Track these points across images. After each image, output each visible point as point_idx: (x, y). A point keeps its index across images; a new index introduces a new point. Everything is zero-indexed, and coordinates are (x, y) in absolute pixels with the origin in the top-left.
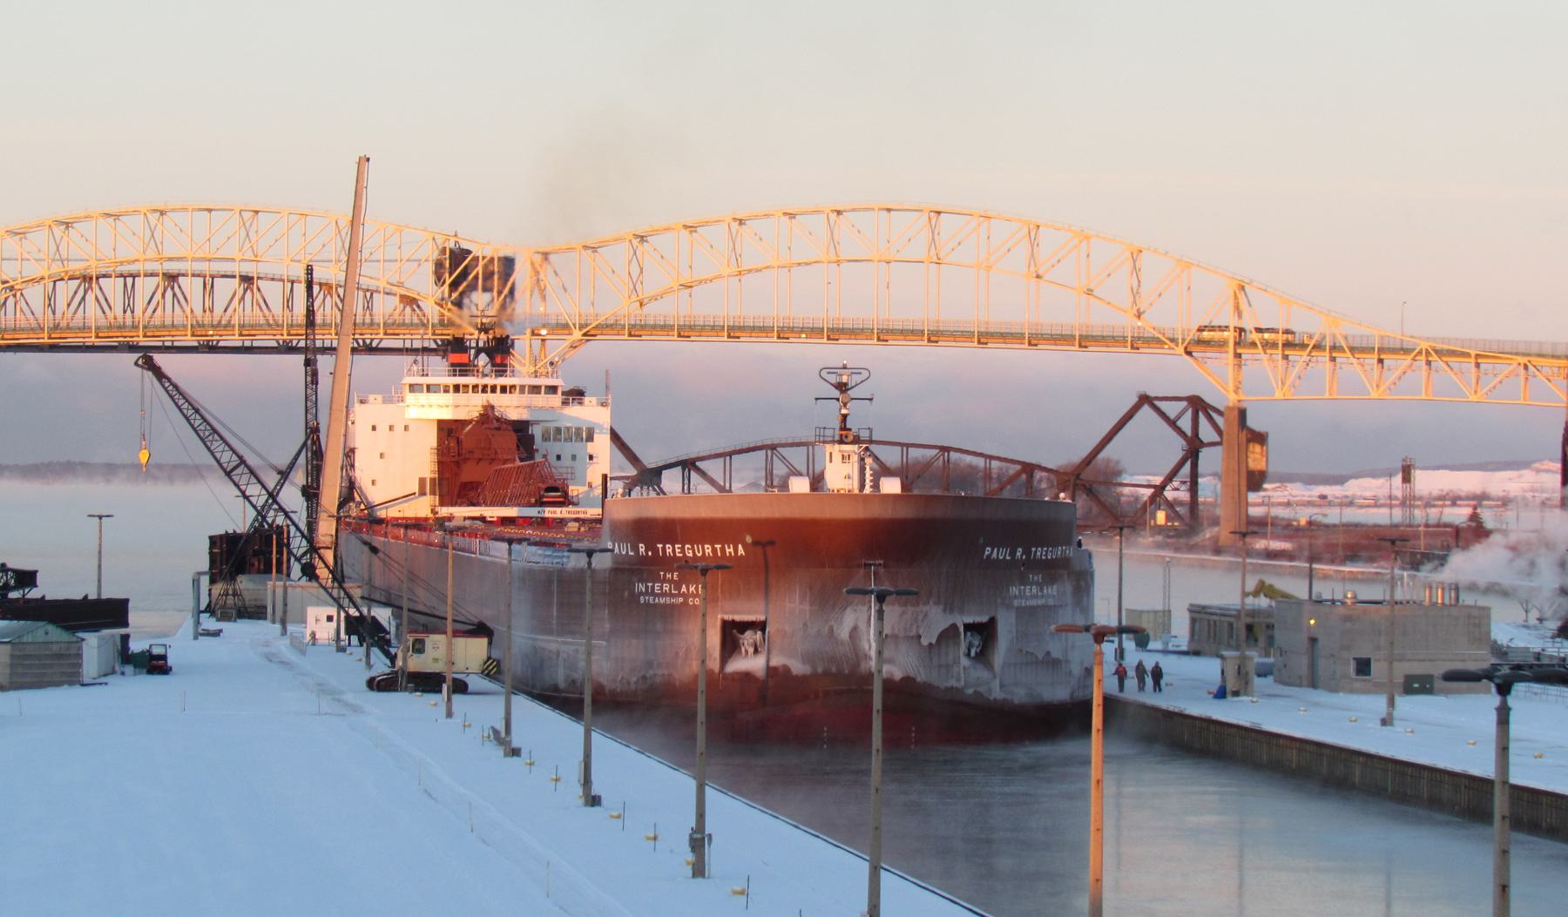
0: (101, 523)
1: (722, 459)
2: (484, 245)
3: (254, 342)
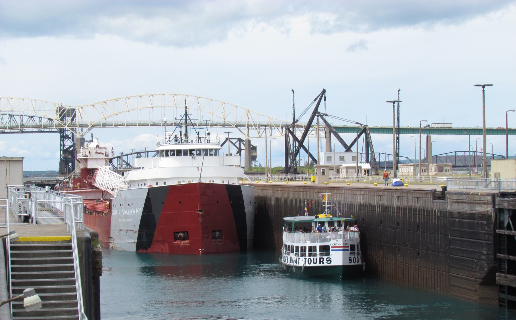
0: (484, 91)
1: (127, 156)
2: (67, 106)
3: (33, 130)
